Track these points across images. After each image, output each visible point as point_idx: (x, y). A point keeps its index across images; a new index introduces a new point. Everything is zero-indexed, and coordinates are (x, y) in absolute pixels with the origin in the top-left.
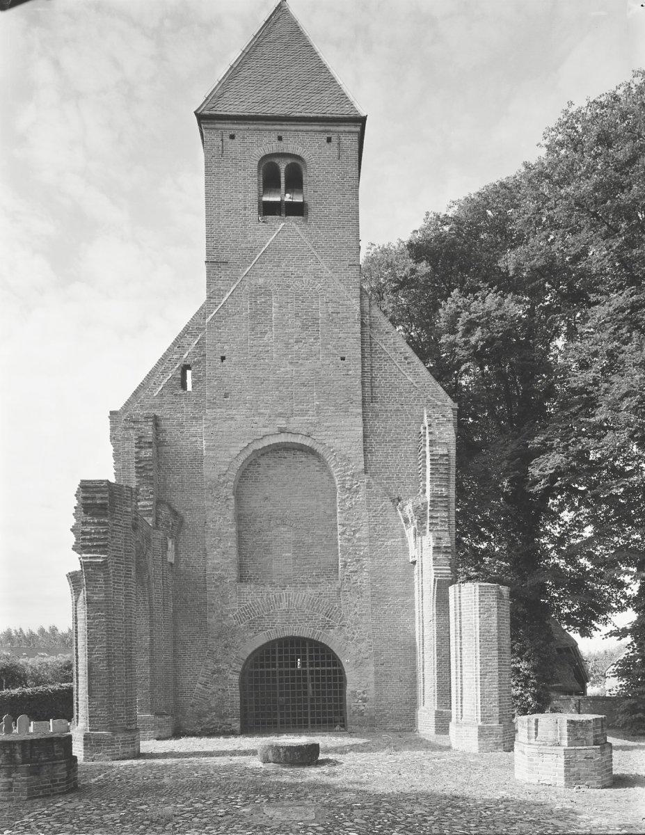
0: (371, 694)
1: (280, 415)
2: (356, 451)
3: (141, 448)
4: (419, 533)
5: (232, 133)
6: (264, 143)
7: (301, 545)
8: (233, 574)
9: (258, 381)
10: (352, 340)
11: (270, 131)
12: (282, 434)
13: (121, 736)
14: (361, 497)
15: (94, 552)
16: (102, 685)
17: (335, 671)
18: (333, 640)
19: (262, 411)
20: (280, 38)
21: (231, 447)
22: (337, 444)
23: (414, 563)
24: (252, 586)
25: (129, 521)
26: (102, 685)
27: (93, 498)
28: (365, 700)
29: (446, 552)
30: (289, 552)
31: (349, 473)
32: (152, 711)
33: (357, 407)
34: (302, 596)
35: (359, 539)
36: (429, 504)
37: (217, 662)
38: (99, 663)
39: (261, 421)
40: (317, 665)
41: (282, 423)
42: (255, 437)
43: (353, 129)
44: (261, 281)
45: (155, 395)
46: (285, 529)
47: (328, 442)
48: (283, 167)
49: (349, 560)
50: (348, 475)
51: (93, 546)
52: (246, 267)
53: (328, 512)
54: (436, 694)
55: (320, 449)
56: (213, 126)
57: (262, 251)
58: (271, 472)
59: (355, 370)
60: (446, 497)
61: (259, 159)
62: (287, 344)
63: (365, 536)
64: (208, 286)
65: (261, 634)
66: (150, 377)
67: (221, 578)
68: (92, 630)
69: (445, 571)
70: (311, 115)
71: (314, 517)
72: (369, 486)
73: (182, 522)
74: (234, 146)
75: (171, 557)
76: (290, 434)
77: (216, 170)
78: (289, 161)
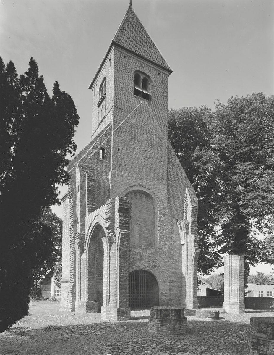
0: (167, 294)
1: (139, 178)
2: (165, 198)
4: (187, 233)
7: (142, 232)
9: (132, 163)
11: (139, 61)
12: (140, 186)
16: (124, 287)
18: (156, 272)
19: (133, 175)
20: (131, 22)
21: (121, 187)
23: (183, 244)
26: (124, 287)
27: (123, 205)
28: (165, 296)
30: (138, 235)
31: (162, 207)
35: (165, 233)
36: (190, 223)
38: (123, 278)
41: (140, 182)
42: (130, 186)
44: (134, 121)
45: (89, 158)
46: (137, 225)
47: (156, 193)
49: (162, 241)
50: (162, 208)
51: (124, 226)
52: (129, 114)
53: (152, 221)
54: (193, 294)
55: (153, 195)
56: (118, 49)
57: (135, 109)
59: (165, 167)
61: (134, 71)
62: (143, 150)
68: (121, 263)
71: (148, 222)
72: (168, 213)
76: (142, 187)
77: (118, 68)
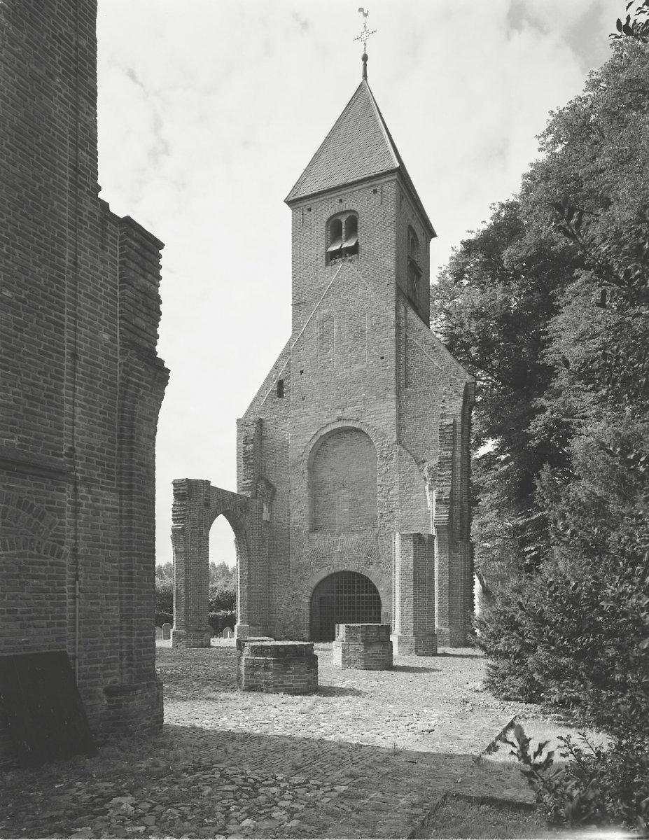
1: (338, 408)
3: (246, 444)
5: (309, 206)
6: (330, 208)
8: (306, 526)
10: (389, 343)
11: (333, 197)
13: (192, 634)
14: (394, 463)
15: (179, 523)
17: (375, 598)
18: (372, 573)
22: (377, 424)
24: (319, 535)
25: (202, 501)
29: (446, 503)
32: (249, 622)
33: (391, 394)
34: (349, 541)
35: (392, 495)
37: (295, 589)
39: (325, 413)
40: (362, 592)
41: (339, 413)
43: (392, 178)
47: (372, 423)
48: (344, 221)
52: (317, 302)
58: (335, 450)
60: (451, 458)
61: (326, 221)
63: (397, 493)
64: (293, 321)
65: (324, 569)
66: (259, 392)
67: (299, 530)
69: (443, 519)
70: (360, 178)
72: (400, 454)
73: (274, 492)
74: (310, 216)
75: (265, 517)
78: (348, 215)
